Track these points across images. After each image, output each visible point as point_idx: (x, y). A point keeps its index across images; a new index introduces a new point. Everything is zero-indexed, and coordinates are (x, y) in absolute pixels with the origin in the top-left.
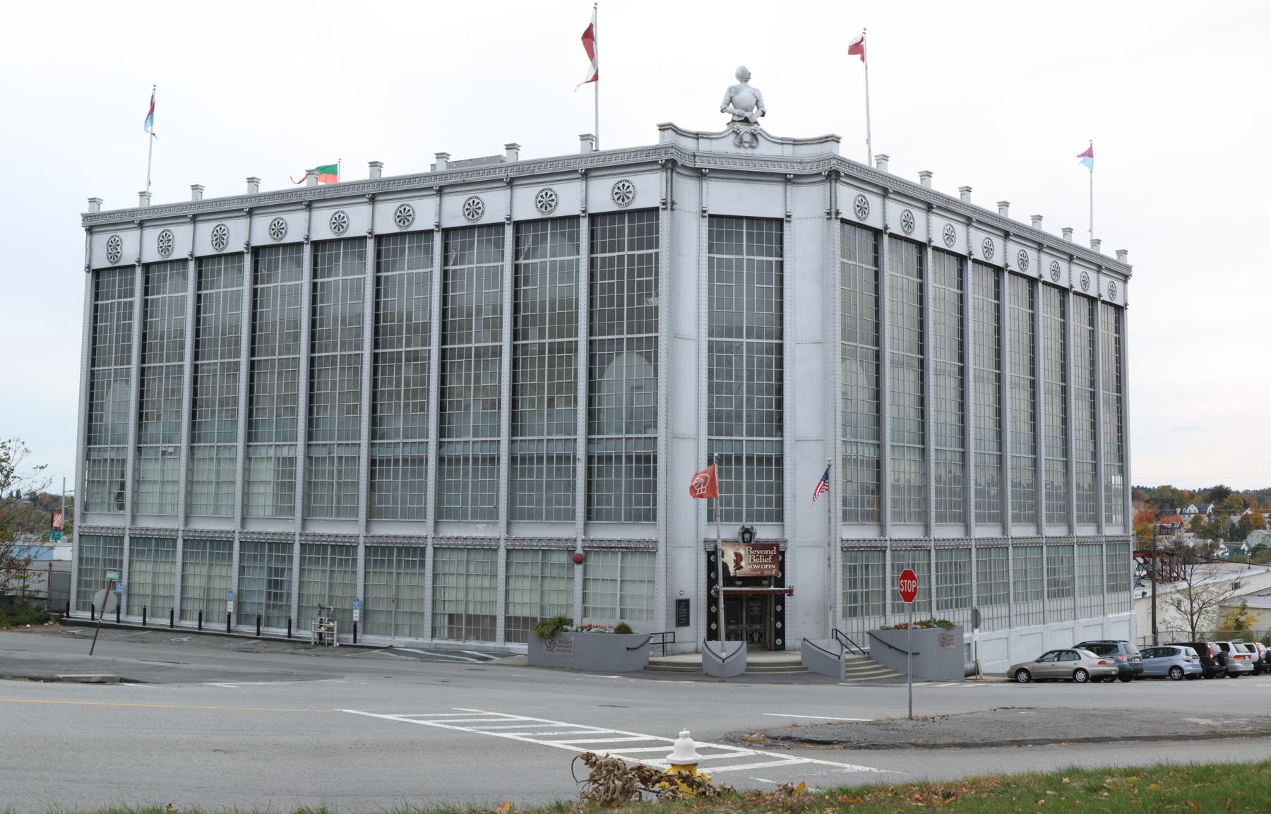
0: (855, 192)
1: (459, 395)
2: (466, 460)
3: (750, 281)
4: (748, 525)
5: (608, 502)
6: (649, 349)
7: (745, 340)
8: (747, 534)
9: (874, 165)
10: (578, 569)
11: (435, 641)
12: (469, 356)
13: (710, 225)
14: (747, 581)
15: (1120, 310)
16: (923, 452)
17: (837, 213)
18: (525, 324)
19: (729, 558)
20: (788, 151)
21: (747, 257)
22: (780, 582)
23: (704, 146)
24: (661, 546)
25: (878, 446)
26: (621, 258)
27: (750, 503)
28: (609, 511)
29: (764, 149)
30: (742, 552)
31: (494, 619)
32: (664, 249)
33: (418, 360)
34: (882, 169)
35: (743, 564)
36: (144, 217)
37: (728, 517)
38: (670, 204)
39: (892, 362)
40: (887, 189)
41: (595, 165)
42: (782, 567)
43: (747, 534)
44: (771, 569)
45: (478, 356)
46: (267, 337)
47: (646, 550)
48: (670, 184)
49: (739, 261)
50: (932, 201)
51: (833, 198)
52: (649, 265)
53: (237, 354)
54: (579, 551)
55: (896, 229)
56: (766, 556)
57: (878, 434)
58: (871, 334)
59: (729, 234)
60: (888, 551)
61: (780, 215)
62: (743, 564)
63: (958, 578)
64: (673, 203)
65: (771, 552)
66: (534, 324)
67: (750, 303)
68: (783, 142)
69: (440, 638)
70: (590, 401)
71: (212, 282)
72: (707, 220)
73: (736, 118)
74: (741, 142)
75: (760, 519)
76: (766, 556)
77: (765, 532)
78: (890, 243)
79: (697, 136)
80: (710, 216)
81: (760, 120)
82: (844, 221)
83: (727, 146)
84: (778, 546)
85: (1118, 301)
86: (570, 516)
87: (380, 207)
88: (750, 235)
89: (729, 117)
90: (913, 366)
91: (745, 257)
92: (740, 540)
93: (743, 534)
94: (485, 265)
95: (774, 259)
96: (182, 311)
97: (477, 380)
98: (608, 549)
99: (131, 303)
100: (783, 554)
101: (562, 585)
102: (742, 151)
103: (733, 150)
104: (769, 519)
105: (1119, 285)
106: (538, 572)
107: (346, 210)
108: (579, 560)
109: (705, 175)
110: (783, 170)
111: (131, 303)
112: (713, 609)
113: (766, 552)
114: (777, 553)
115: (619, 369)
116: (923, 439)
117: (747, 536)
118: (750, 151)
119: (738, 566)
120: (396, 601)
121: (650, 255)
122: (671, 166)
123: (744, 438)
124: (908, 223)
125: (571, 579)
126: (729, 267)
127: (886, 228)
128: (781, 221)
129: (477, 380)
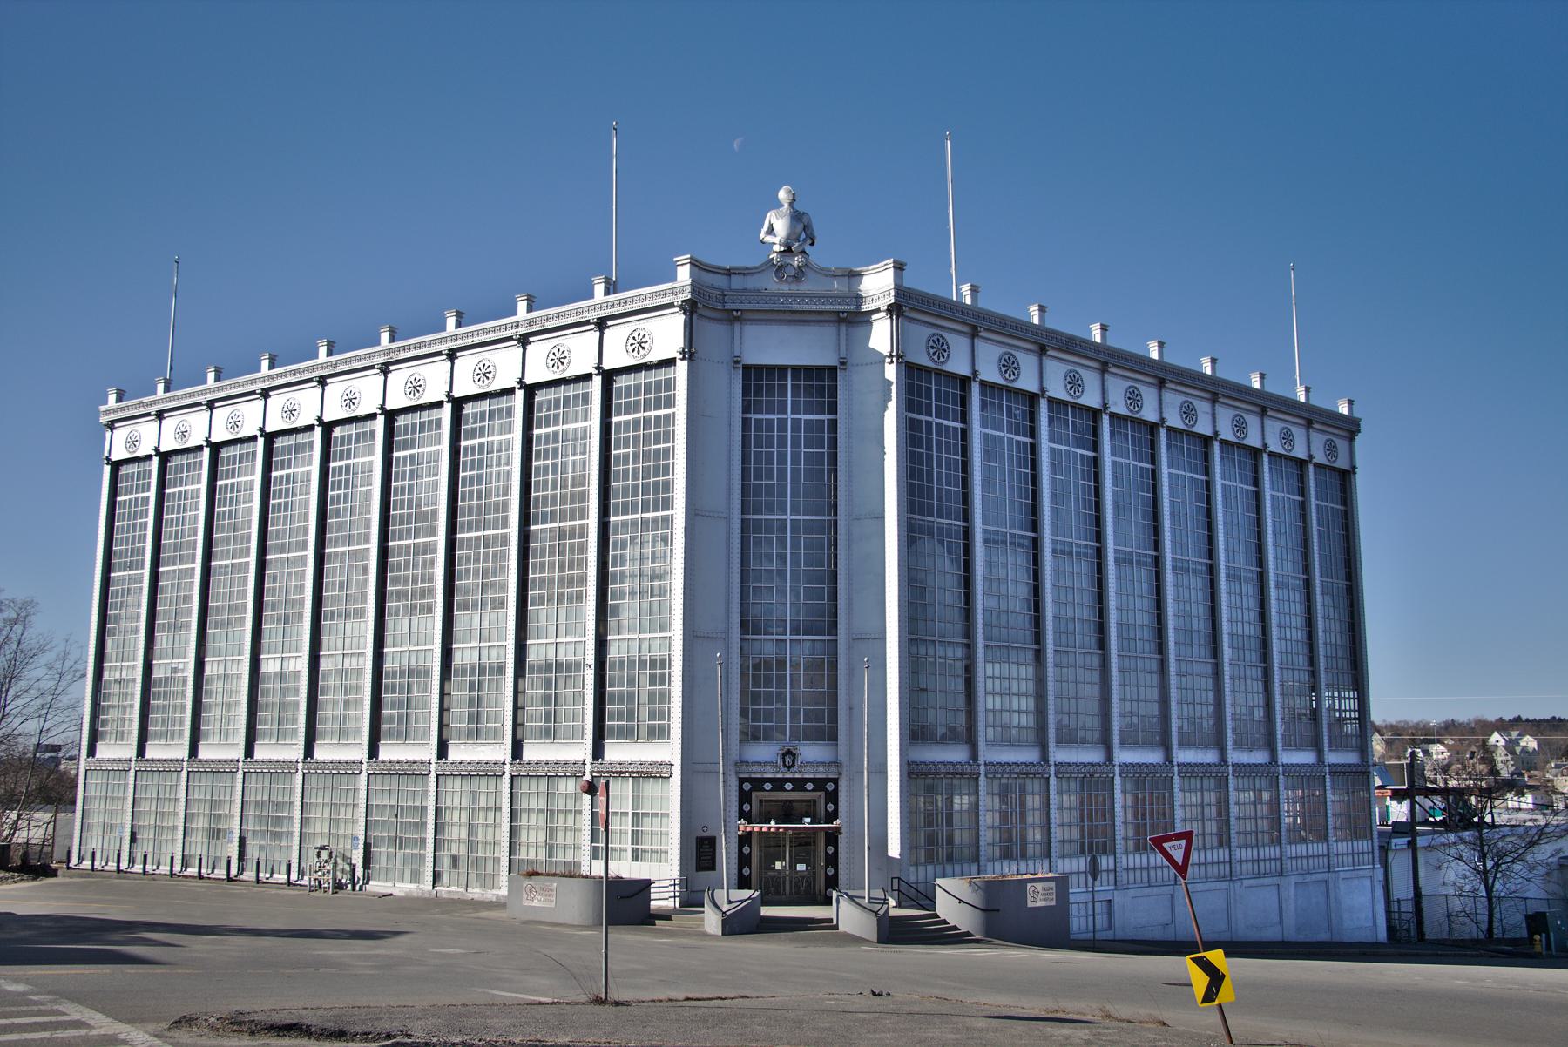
0: (1232, 413)
3: (796, 444)
5: (768, 718)
15: (1345, 478)
16: (1039, 655)
21: (791, 413)
23: (737, 282)
25: (968, 646)
39: (1228, 576)
49: (783, 422)
50: (976, 322)
58: (1205, 547)
59: (770, 389)
60: (982, 778)
61: (828, 359)
63: (278, 821)
67: (796, 472)
78: (1221, 451)
79: (729, 273)
80: (747, 368)
85: (1342, 463)
88: (795, 388)
90: (1145, 564)
91: (790, 416)
92: (780, 762)
93: (784, 755)
95: (825, 417)
98: (620, 773)
104: (820, 738)
105: (1342, 445)
109: (737, 319)
116: (1038, 637)
117: (788, 759)
118: (794, 288)
120: (1141, 869)
121: (667, 417)
123: (788, 637)
128: (833, 370)
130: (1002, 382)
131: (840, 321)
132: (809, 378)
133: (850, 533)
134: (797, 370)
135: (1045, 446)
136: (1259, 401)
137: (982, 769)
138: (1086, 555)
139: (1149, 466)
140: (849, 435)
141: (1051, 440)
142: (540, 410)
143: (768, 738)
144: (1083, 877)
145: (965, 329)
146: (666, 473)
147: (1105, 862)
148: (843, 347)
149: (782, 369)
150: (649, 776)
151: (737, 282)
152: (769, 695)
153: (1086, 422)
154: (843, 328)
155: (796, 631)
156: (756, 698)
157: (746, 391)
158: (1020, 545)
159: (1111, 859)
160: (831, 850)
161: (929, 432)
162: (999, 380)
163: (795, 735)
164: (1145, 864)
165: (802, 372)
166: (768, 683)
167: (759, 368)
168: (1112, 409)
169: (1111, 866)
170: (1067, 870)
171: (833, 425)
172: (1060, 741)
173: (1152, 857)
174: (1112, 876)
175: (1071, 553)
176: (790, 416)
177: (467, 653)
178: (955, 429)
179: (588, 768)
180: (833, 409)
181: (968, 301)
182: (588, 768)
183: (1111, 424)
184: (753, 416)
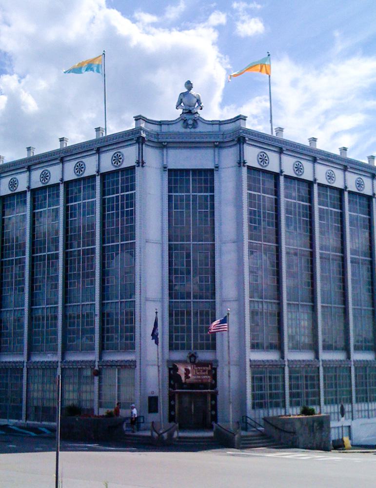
0: (258, 151)
1: (40, 282)
2: (78, 316)
4: (193, 351)
5: (183, 339)
6: (130, 249)
7: (191, 242)
8: (193, 356)
9: (274, 134)
10: (96, 379)
11: (28, 422)
12: (79, 255)
13: (169, 176)
14: (192, 386)
16: (314, 308)
17: (244, 163)
18: (71, 240)
19: (182, 370)
20: (216, 128)
22: (214, 386)
23: (165, 128)
24: (138, 364)
26: (117, 197)
27: (189, 337)
28: (183, 344)
29: (201, 128)
30: (190, 368)
31: (55, 409)
32: (138, 191)
33: (21, 262)
34: (279, 137)
35: (190, 375)
36: (99, 145)
37: (183, 347)
38: (141, 163)
40: (282, 147)
41: (102, 144)
42: (214, 377)
43: (193, 356)
44: (207, 378)
45: (48, 259)
46: (41, 241)
47: (130, 365)
48: (141, 153)
51: (241, 153)
52: (130, 201)
53: (93, 243)
54: (97, 368)
55: (352, 187)
56: (204, 371)
57: (279, 297)
59: (181, 181)
61: (211, 166)
62: (190, 375)
64: (143, 163)
65: (207, 368)
66: (75, 240)
68: (212, 123)
69: (30, 421)
70: (103, 281)
71: (41, 204)
72: (167, 172)
73: (184, 112)
74: (188, 125)
75: (202, 349)
76: (204, 371)
77: (204, 356)
78: (285, 181)
79: (160, 123)
80: (170, 171)
81: (199, 111)
82: (250, 168)
83: (179, 128)
84: (212, 365)
86: (92, 349)
87: (103, 156)
89: (180, 111)
91: (191, 194)
92: (188, 361)
94: (125, 193)
95: (208, 194)
96: (93, 212)
97: (48, 274)
98: (112, 365)
99: (26, 215)
100: (215, 369)
101: (88, 388)
102: (188, 130)
103: (183, 130)
104: (208, 348)
106: (76, 380)
107: (122, 150)
108: (98, 373)
109: (165, 147)
110: (212, 140)
111: (26, 215)
112: (213, 402)
113: (204, 368)
114: (212, 368)
115: (117, 261)
116: (313, 299)
117: (192, 359)
118: (193, 130)
119: (187, 377)
120: (365, 410)
122: (140, 141)
124: (298, 168)
125: (93, 383)
126: (182, 200)
127: (315, 180)
128: (211, 171)
129: (48, 274)
130: (295, 176)
131: (216, 146)
132: (200, 175)
133: (220, 250)
134: (195, 171)
135: (347, 213)
136: (312, 154)
137: (286, 363)
138: (303, 255)
139: (339, 211)
140: (220, 203)
141: (319, 204)
142: (72, 194)
143: (183, 348)
144: (336, 415)
145: (310, 159)
146: (132, 222)
147: (347, 407)
148: (217, 159)
149: (187, 171)
150: (125, 366)
151: (165, 128)
152: (182, 328)
153: (365, 202)
154: (217, 150)
155: (195, 297)
156: (177, 330)
157: (169, 182)
158: (365, 264)
159: (350, 406)
160: (213, 402)
161: (259, 200)
162: (326, 183)
163: (195, 348)
164: (360, 409)
165: (197, 172)
166: (183, 323)
167: (176, 171)
168: (317, 181)
169: (350, 410)
170: (329, 411)
171: (212, 197)
172: (324, 348)
173: (271, 411)
174: (350, 414)
175: (329, 259)
176: (191, 194)
177: (40, 311)
178: (307, 206)
179: (97, 364)
180: (212, 190)
181: (274, 134)
182: (97, 364)
183: (349, 197)
184: (173, 194)
